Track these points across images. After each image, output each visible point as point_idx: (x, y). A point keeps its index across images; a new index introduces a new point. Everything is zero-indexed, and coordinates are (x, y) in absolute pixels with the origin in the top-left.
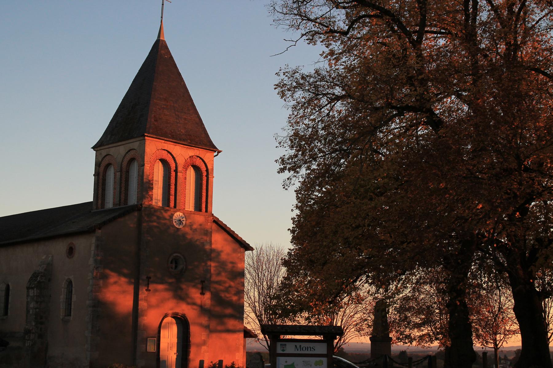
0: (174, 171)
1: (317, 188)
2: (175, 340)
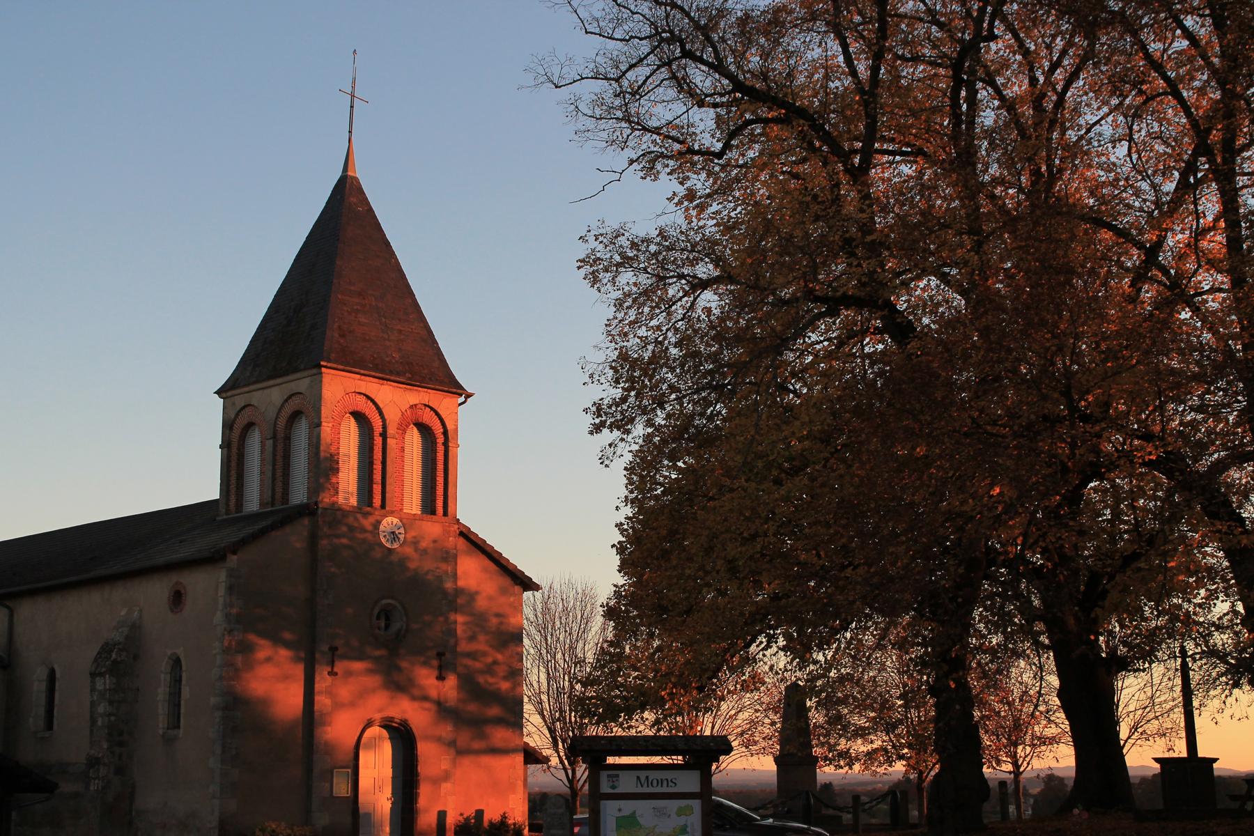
1: (666, 462)
2: (389, 772)
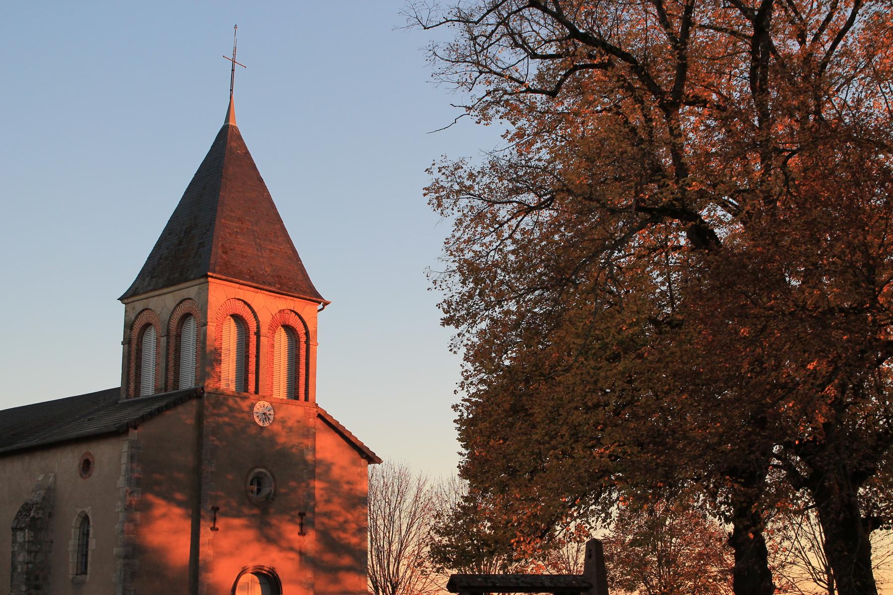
0: (255, 334)
